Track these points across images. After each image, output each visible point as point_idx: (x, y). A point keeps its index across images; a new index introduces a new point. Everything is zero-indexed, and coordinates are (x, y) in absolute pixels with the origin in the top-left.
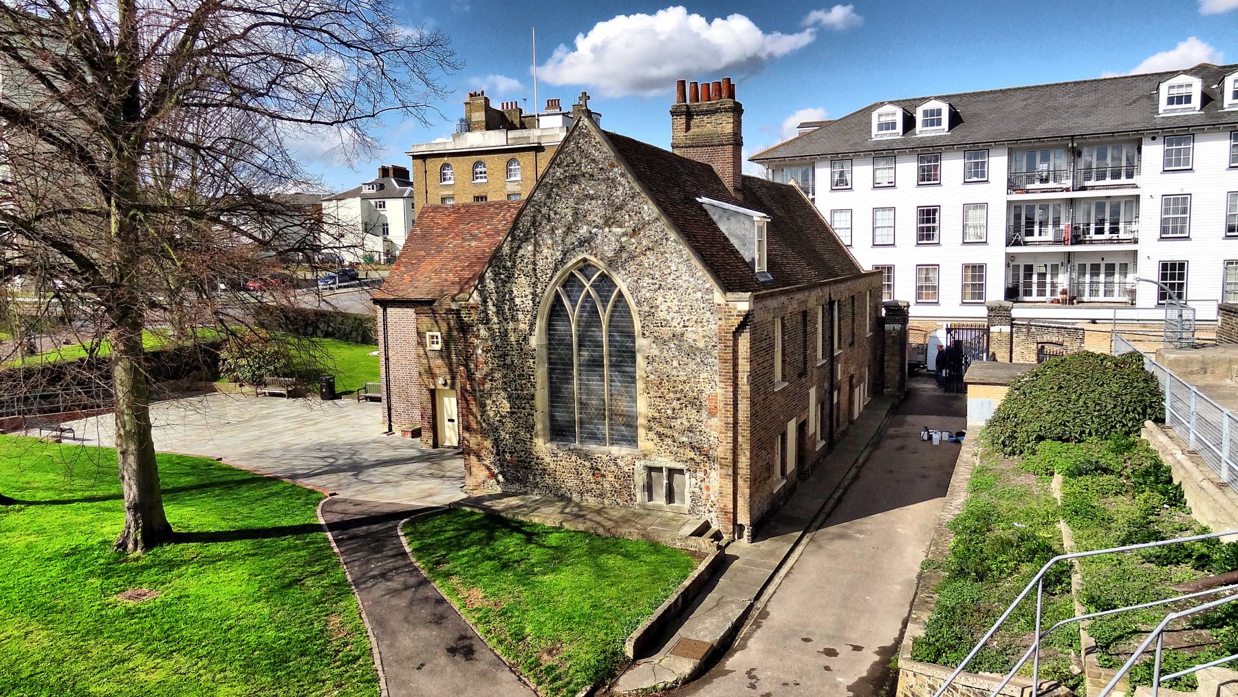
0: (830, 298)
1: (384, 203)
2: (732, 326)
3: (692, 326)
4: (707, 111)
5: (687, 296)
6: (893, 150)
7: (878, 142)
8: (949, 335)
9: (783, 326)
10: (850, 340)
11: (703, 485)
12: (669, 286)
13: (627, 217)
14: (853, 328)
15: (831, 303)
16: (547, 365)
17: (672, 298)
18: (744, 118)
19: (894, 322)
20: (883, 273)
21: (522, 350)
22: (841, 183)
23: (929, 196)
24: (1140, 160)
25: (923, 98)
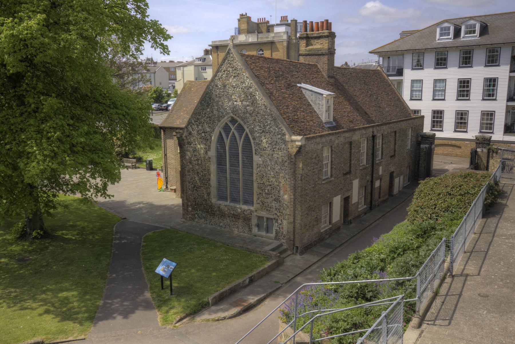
1: (205, 68)
11: (281, 226)
15: (374, 137)
19: (426, 143)
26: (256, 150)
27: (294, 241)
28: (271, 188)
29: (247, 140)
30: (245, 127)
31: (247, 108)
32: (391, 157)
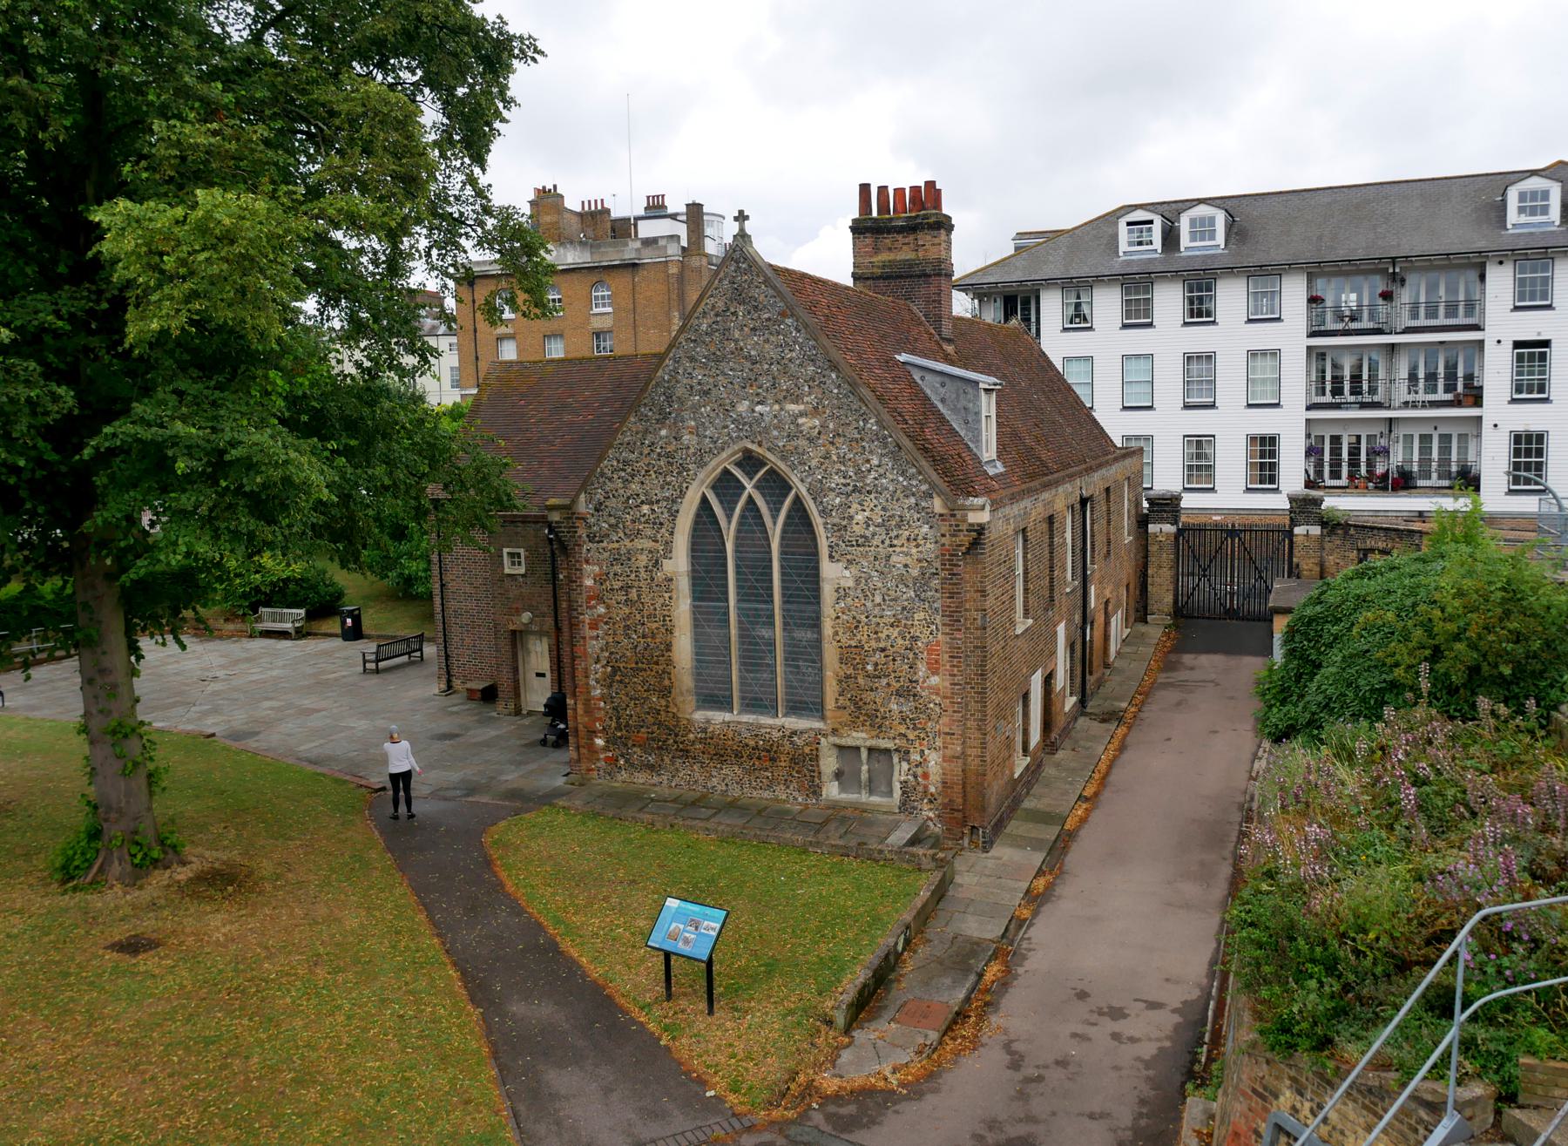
3: (903, 545)
7: (1129, 263)
13: (806, 389)
14: (1108, 533)
16: (689, 601)
17: (872, 505)
19: (1162, 520)
20: (1136, 451)
21: (652, 579)
22: (1078, 319)
23: (1200, 339)
24: (1483, 292)
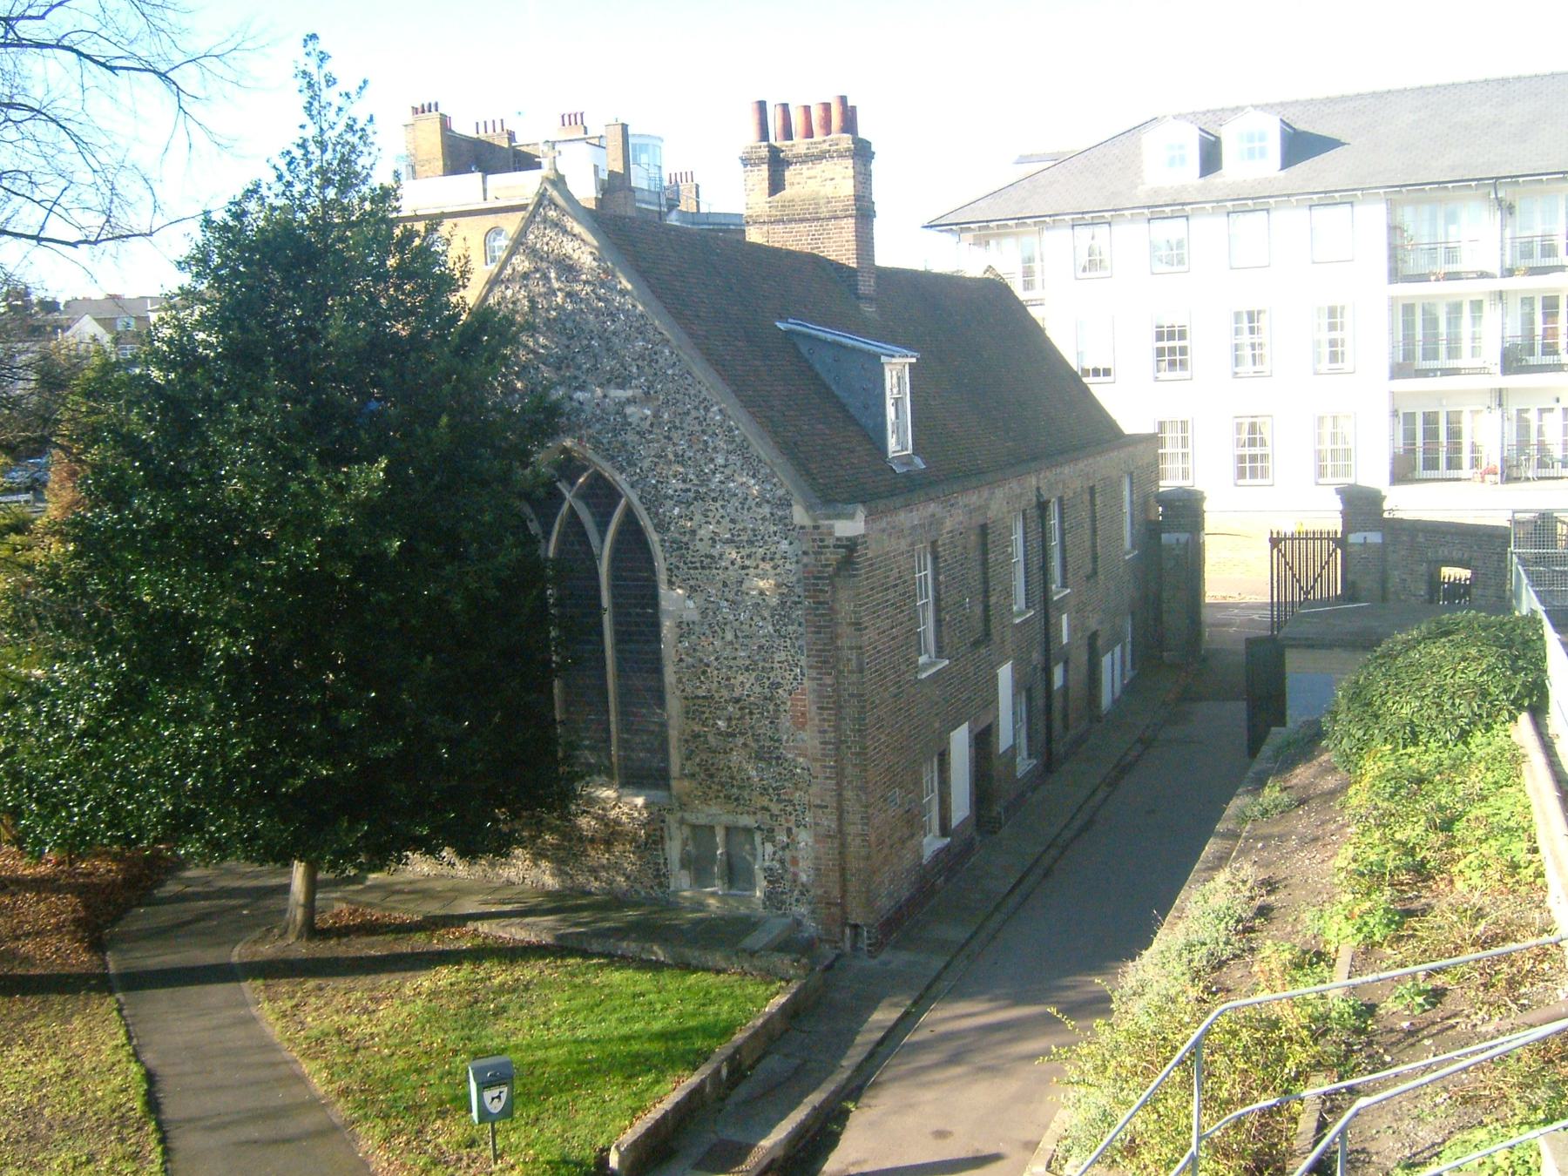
0: (1039, 495)
2: (826, 566)
4: (806, 155)
5: (745, 512)
6: (1183, 204)
8: (1275, 551)
9: (1132, 483)
10: (1088, 568)
11: (788, 854)
12: (713, 495)
15: (1043, 506)
18: (875, 166)
25: (1237, 108)
26: (668, 569)
27: (842, 906)
28: (741, 709)
29: (632, 535)
30: (621, 480)
31: (629, 410)
32: (1088, 578)
